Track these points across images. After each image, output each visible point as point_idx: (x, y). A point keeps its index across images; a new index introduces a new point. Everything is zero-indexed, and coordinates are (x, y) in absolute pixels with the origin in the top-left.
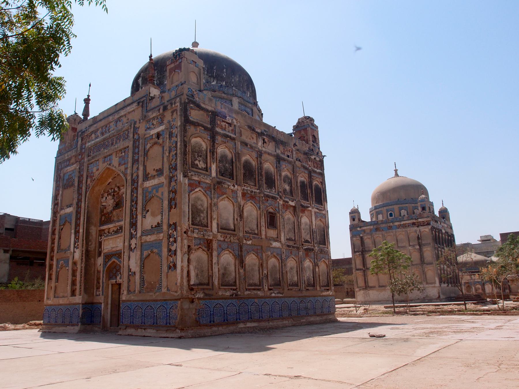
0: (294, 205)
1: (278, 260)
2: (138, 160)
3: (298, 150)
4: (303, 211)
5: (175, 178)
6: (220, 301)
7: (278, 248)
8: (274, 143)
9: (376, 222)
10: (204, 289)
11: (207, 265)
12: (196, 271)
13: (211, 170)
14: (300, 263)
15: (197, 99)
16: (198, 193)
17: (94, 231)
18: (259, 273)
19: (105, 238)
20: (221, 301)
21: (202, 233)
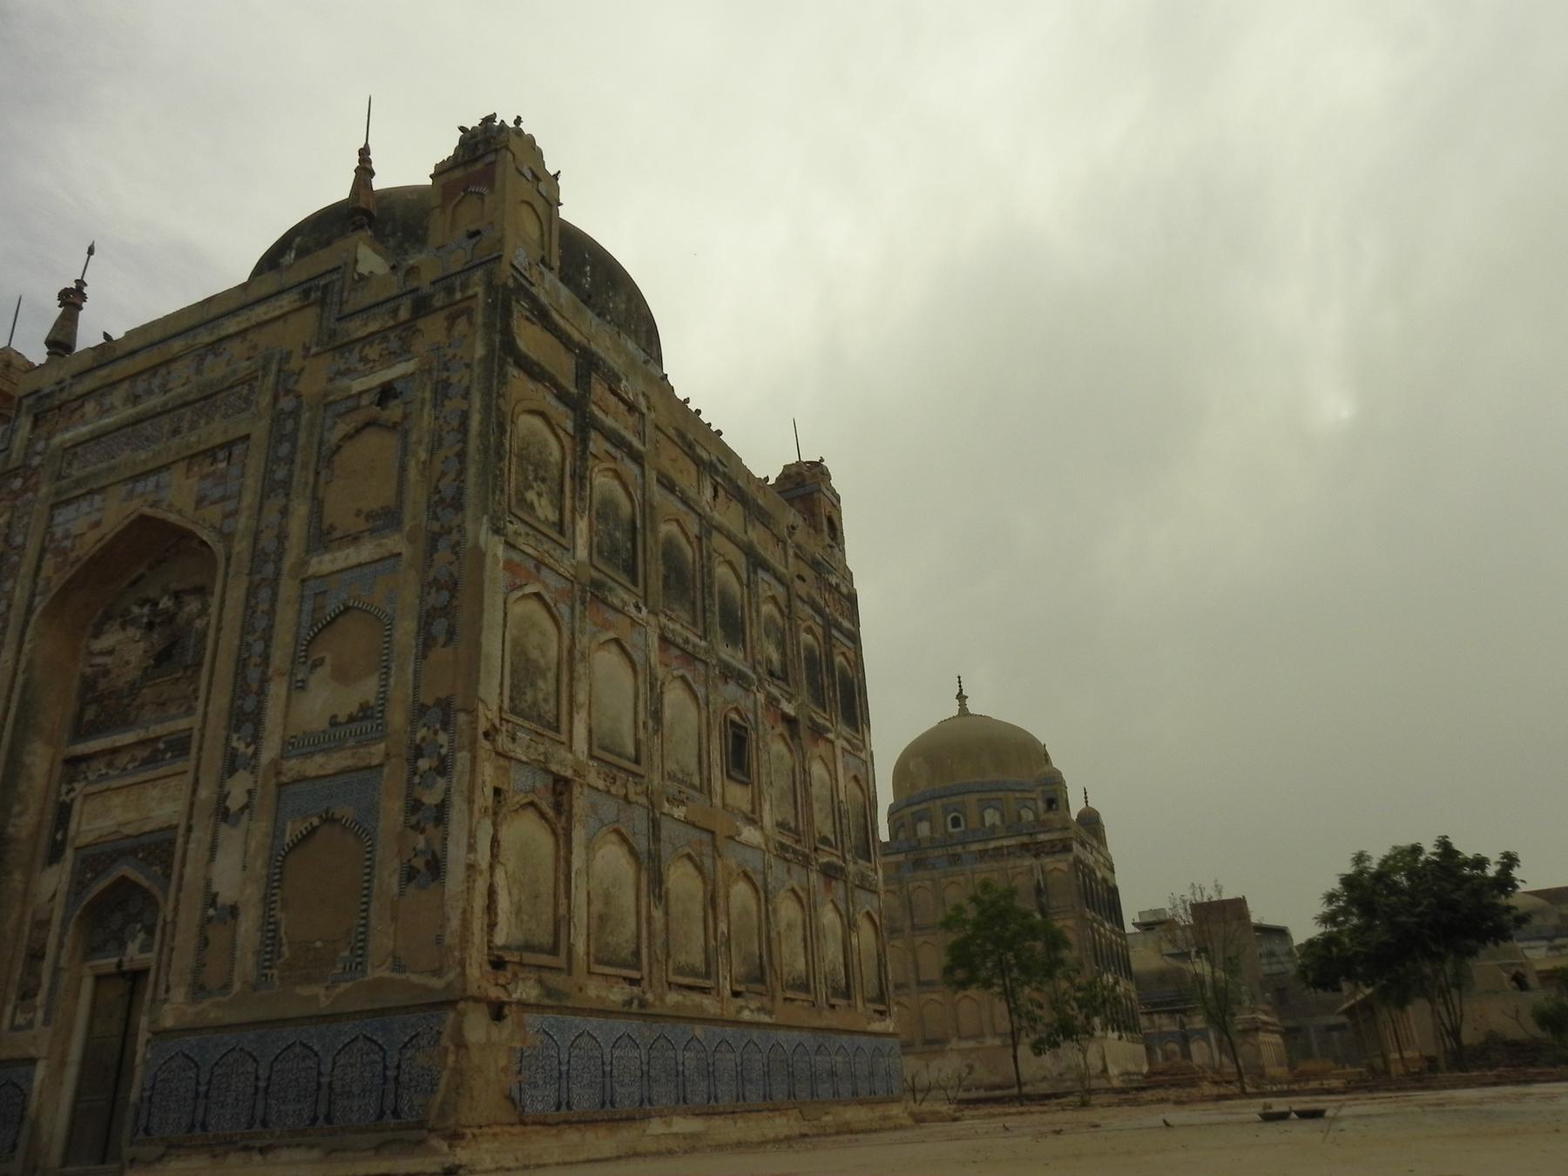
0: (792, 713)
5: (455, 536)
6: (591, 1024)
7: (757, 848)
10: (540, 967)
12: (515, 891)
18: (706, 928)
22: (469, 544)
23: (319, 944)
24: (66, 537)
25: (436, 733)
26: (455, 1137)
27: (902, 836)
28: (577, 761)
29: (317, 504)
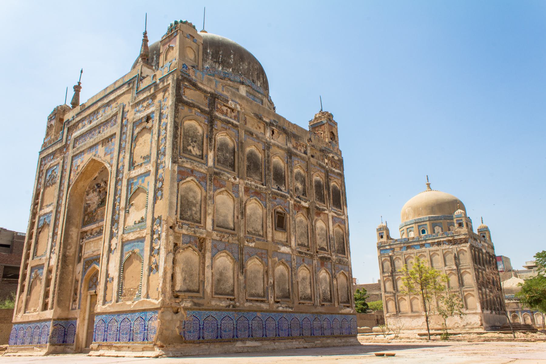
0: (307, 206)
1: (288, 268)
2: (125, 148)
3: (313, 146)
4: (318, 214)
5: (163, 165)
6: (213, 313)
8: (285, 136)
10: (192, 297)
12: (183, 274)
13: (207, 158)
14: (314, 273)
15: (194, 77)
16: (190, 183)
17: (74, 233)
18: (264, 281)
19: (86, 241)
20: (214, 312)
21: (193, 229)
28: (207, 231)
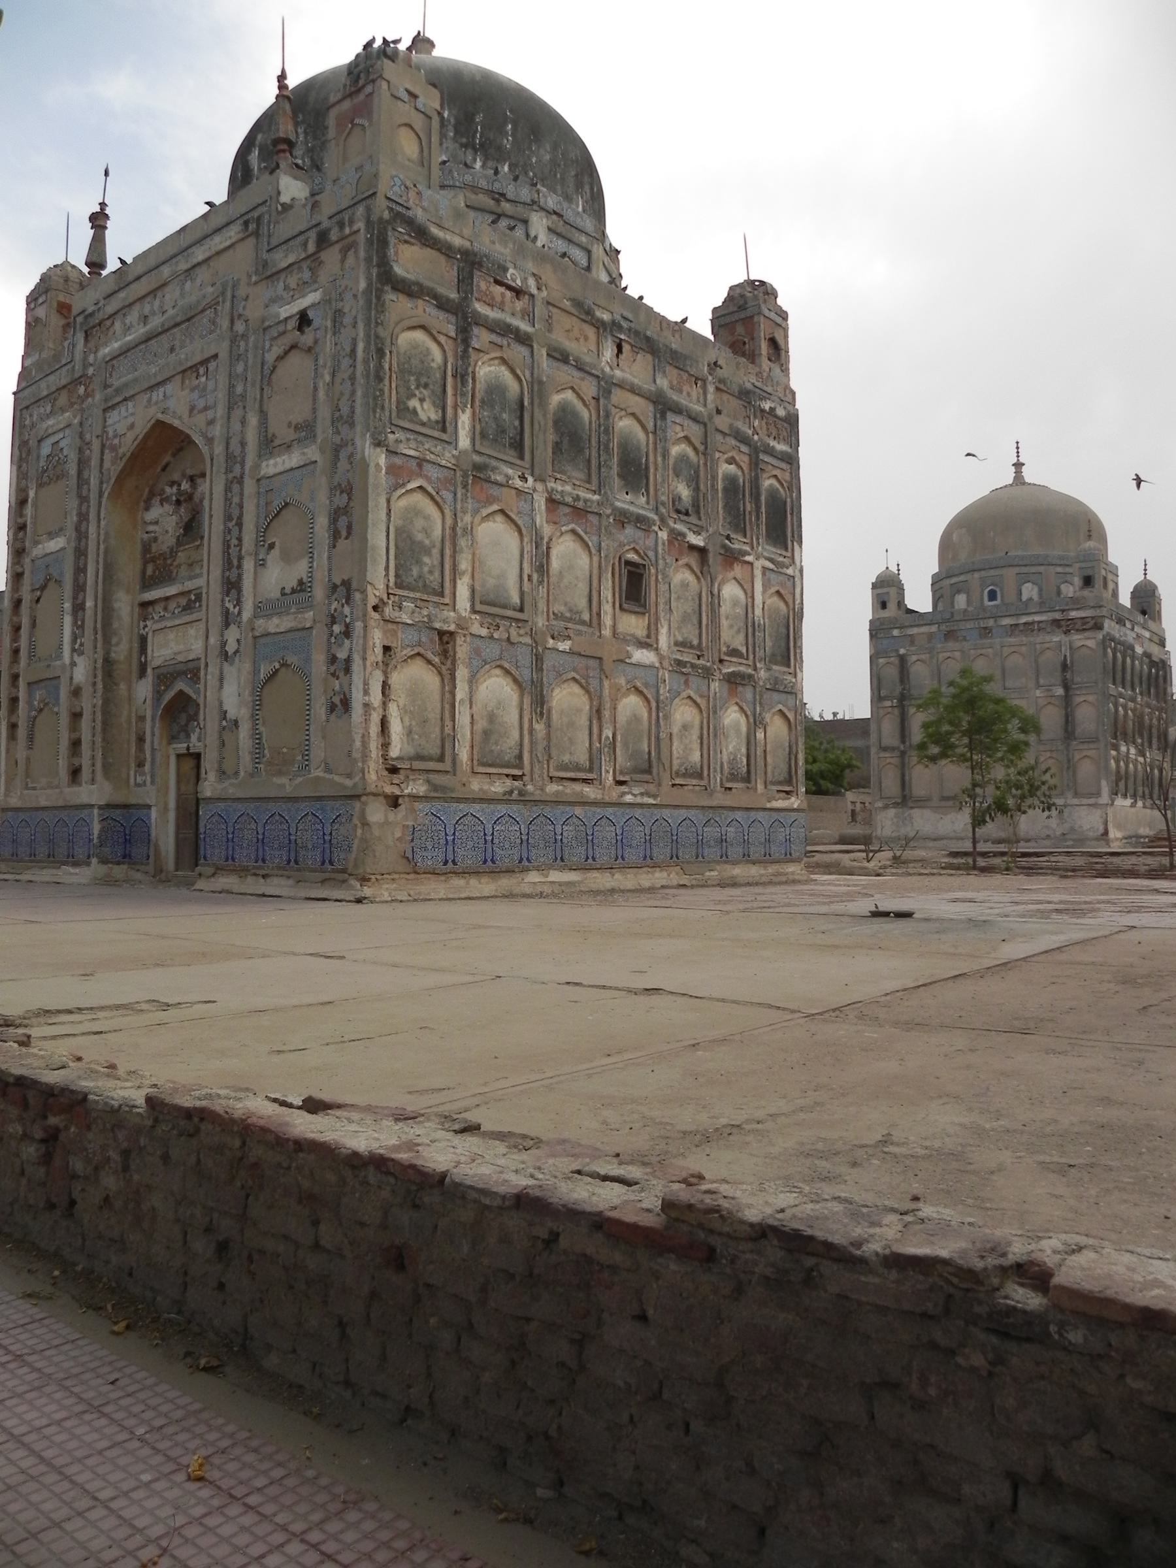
0: (702, 544)
2: (243, 397)
5: (350, 449)
6: (475, 808)
7: (651, 667)
8: (649, 357)
9: (948, 616)
10: (428, 771)
11: (439, 705)
12: (406, 719)
14: (710, 714)
17: (124, 605)
22: (358, 457)
23: (285, 750)
24: (115, 436)
25: (343, 606)
26: (364, 880)
27: (940, 607)
28: (460, 618)
29: (263, 414)
